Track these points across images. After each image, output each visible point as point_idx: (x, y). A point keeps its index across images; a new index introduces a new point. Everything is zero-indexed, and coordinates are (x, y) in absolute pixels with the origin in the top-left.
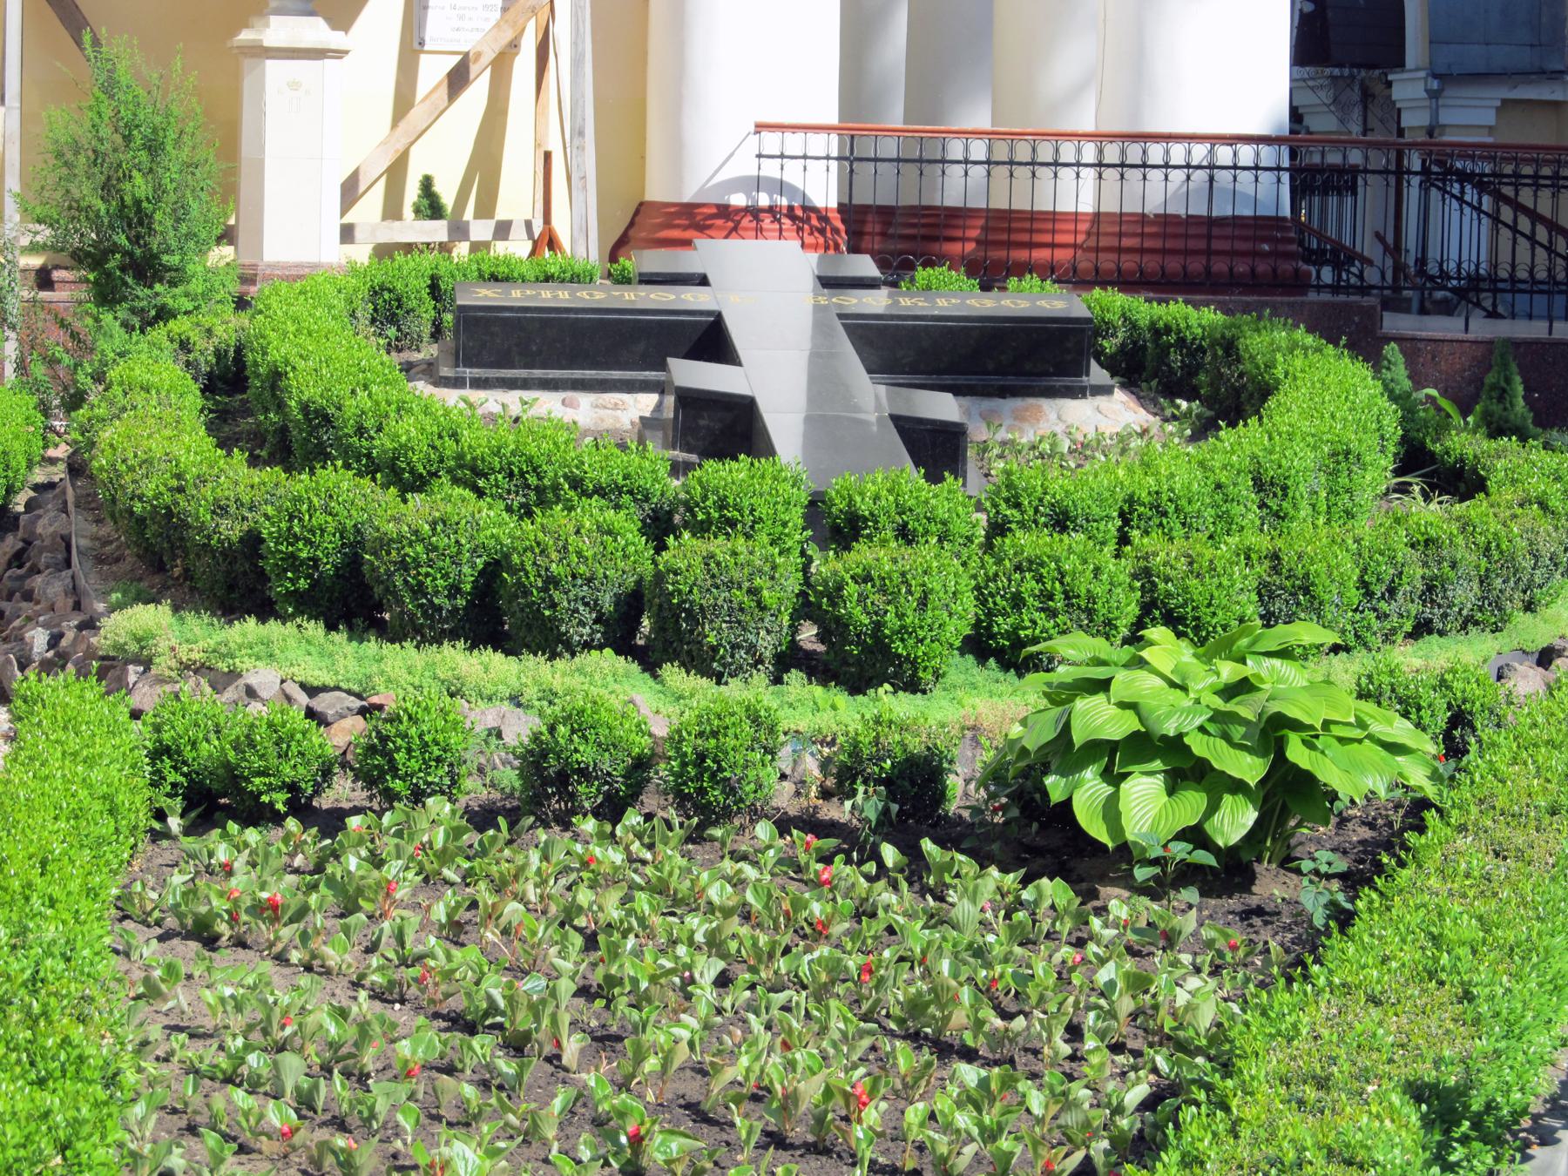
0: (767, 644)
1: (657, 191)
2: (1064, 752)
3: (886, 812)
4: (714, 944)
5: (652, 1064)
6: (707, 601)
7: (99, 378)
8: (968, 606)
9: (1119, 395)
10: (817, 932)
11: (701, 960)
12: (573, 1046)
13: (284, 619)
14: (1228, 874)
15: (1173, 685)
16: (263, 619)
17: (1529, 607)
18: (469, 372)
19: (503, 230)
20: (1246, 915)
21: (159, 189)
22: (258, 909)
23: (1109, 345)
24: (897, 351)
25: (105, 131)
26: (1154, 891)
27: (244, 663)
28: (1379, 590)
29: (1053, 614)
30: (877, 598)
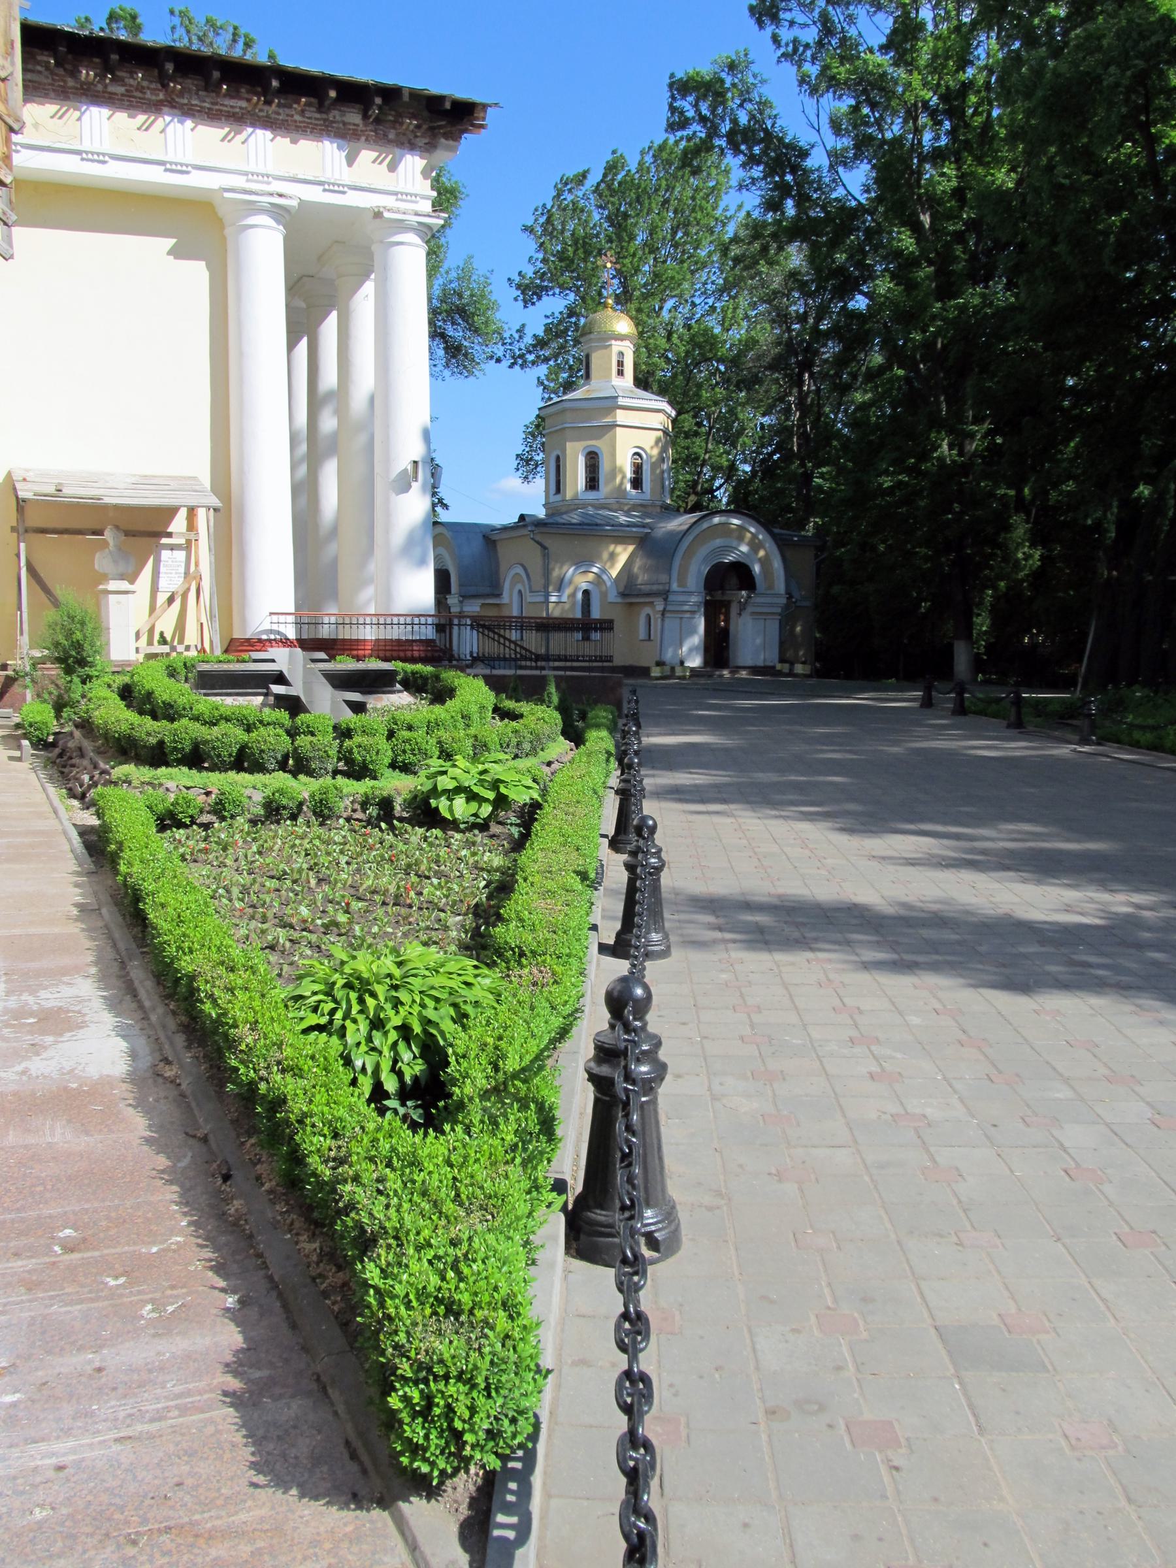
0: (330, 768)
1: (236, 636)
2: (434, 792)
3: (379, 814)
4: (342, 852)
8: (390, 753)
10: (371, 848)
12: (313, 882)
14: (484, 827)
17: (542, 750)
19: (188, 648)
20: (492, 836)
21: (85, 636)
22: (200, 851)
23: (399, 678)
24: (341, 681)
26: (463, 832)
27: (163, 781)
29: (415, 755)
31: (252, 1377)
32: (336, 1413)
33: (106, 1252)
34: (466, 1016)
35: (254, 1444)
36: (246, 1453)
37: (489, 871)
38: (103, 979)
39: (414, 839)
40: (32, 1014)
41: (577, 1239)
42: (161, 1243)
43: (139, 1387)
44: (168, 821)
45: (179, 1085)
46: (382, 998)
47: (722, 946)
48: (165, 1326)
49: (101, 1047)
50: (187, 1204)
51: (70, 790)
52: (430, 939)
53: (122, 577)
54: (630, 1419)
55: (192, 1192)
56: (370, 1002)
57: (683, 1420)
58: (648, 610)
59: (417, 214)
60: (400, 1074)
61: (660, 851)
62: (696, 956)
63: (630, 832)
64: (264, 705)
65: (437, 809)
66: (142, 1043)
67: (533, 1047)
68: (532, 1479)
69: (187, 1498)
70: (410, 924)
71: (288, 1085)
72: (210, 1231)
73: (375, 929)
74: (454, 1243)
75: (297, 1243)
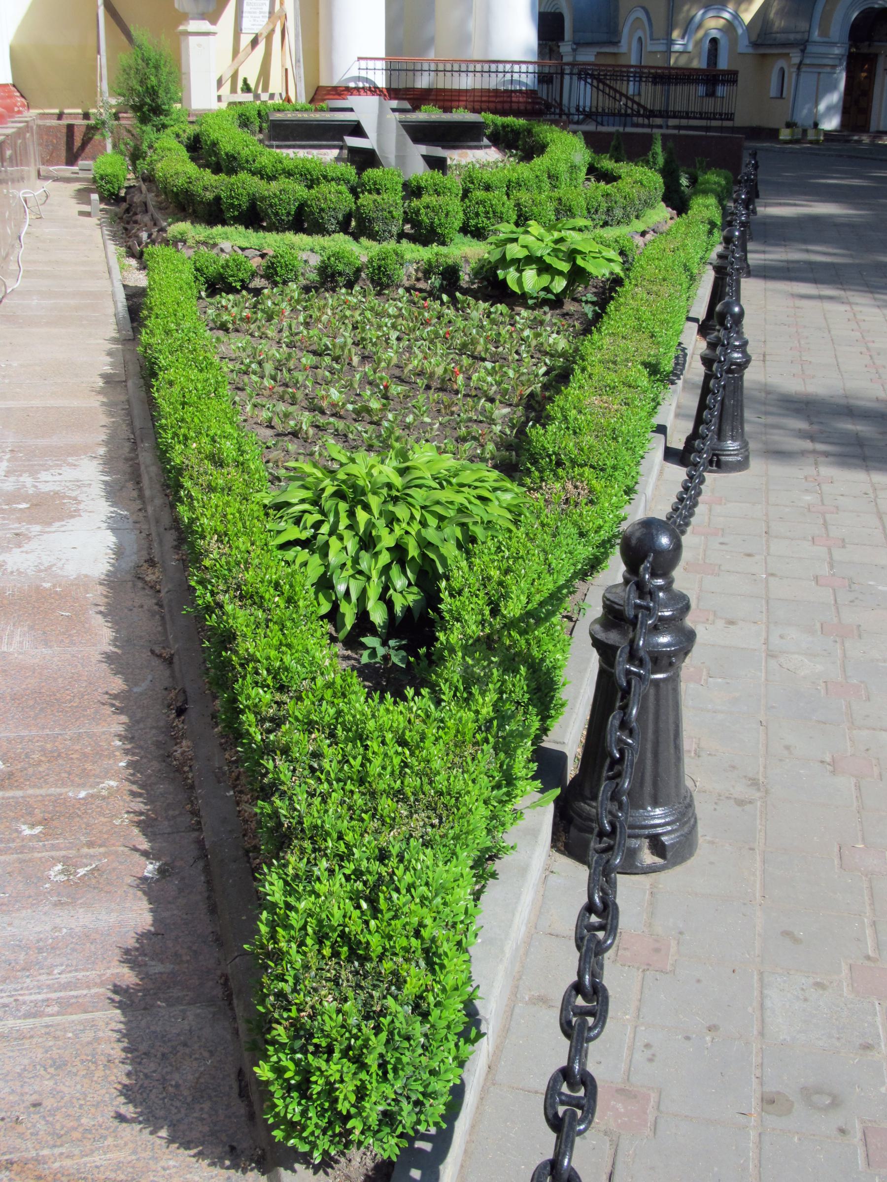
0: (395, 230)
1: (324, 83)
3: (442, 285)
4: (394, 326)
5: (383, 364)
6: (375, 215)
7: (150, 147)
8: (461, 215)
9: (493, 149)
10: (426, 323)
11: (392, 332)
12: (356, 360)
13: (231, 225)
14: (556, 303)
16: (223, 225)
17: (637, 217)
18: (275, 143)
19: (272, 96)
20: (564, 315)
21: (159, 81)
22: (242, 319)
23: (488, 132)
24: (420, 133)
25: (140, 62)
26: (532, 308)
27: (218, 241)
28: (592, 211)
29: (489, 219)
30: (432, 214)
31: (152, 971)
32: (236, 1032)
33: (31, 791)
34: (473, 540)
35: (133, 1061)
36: (120, 1074)
37: (552, 356)
38: (109, 462)
39: (475, 315)
40: (25, 498)
41: (567, 831)
42: (92, 787)
43: (24, 969)
44: (217, 285)
45: (159, 591)
46: (376, 512)
47: (811, 459)
48: (73, 892)
49: (87, 544)
50: (131, 739)
51: (129, 248)
52: (469, 433)
53: (202, 16)
54: (558, 1138)
55: (142, 726)
56: (362, 516)
57: (653, 1097)
58: (781, 63)
60: (390, 604)
61: (745, 343)
62: (778, 470)
63: (721, 320)
64: (338, 159)
65: (504, 280)
66: (132, 539)
67: (549, 585)
68: (441, 1167)
69: (41, 1126)
70: (452, 413)
71: (239, 617)
72: (150, 776)
73: (410, 419)
74: (383, 856)
75: (238, 804)
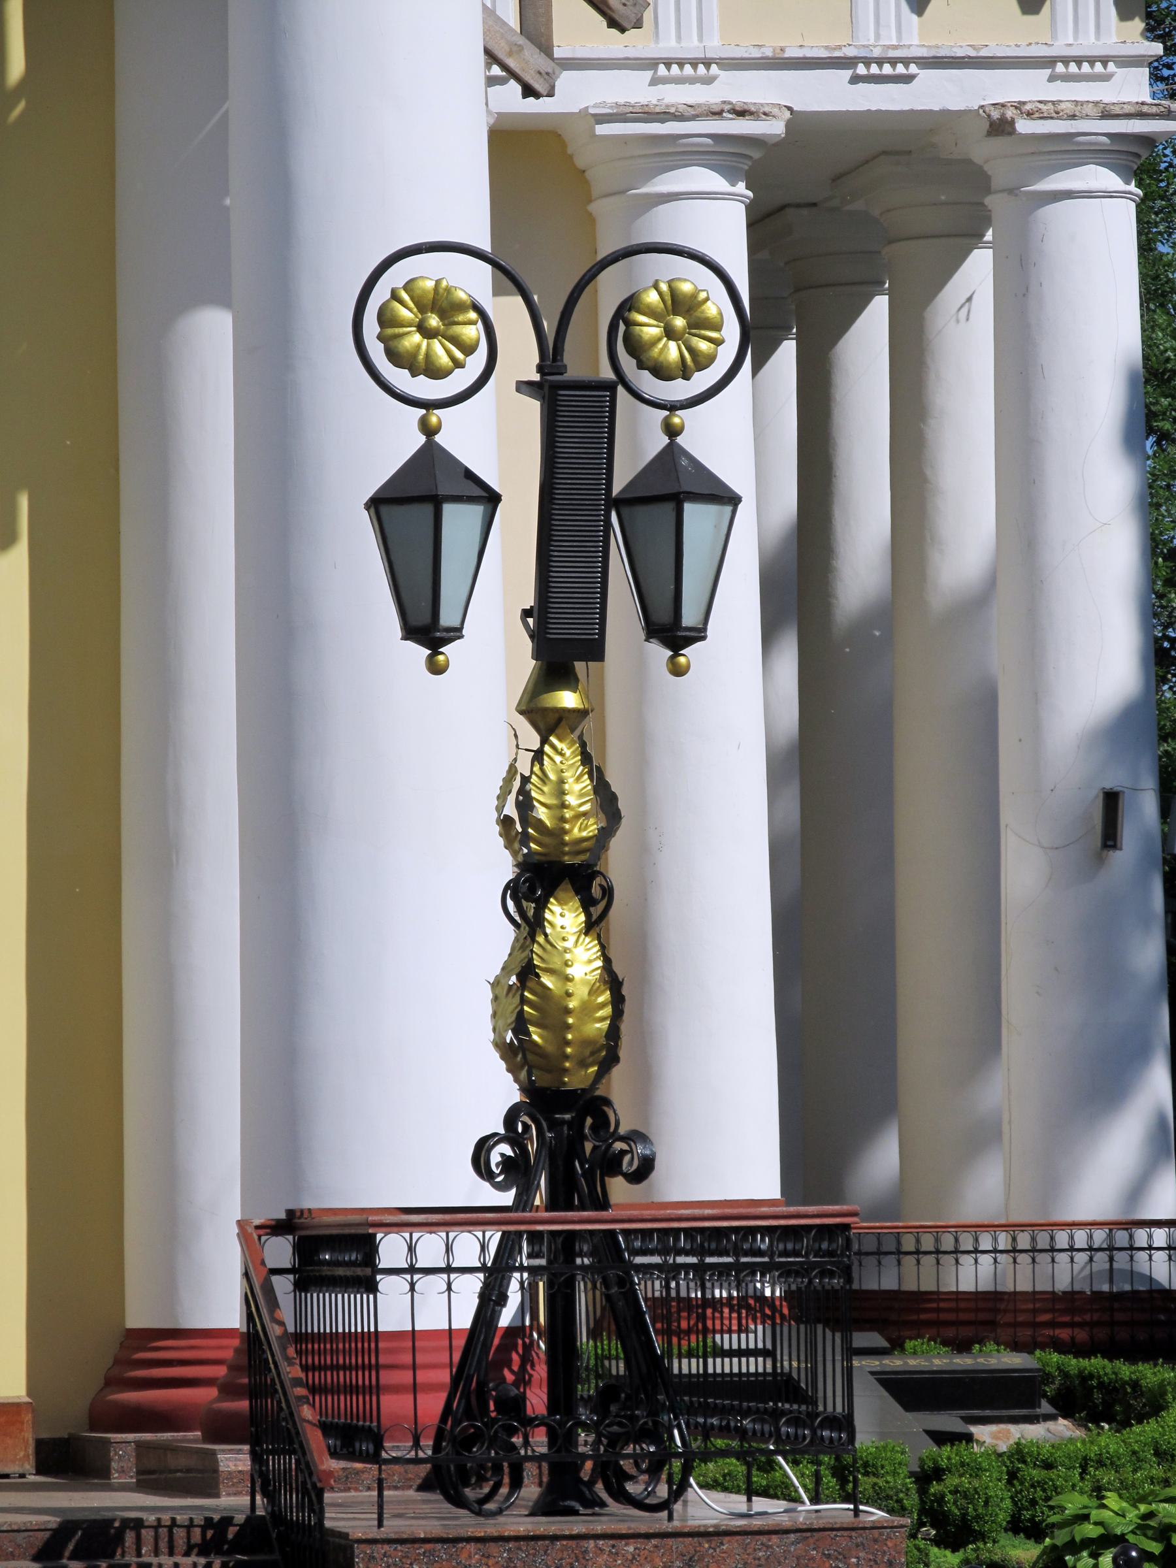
8: (1008, 1503)
15: (1117, 1514)
23: (1049, 1390)
59: (1106, 115)
68: (842, 343)
